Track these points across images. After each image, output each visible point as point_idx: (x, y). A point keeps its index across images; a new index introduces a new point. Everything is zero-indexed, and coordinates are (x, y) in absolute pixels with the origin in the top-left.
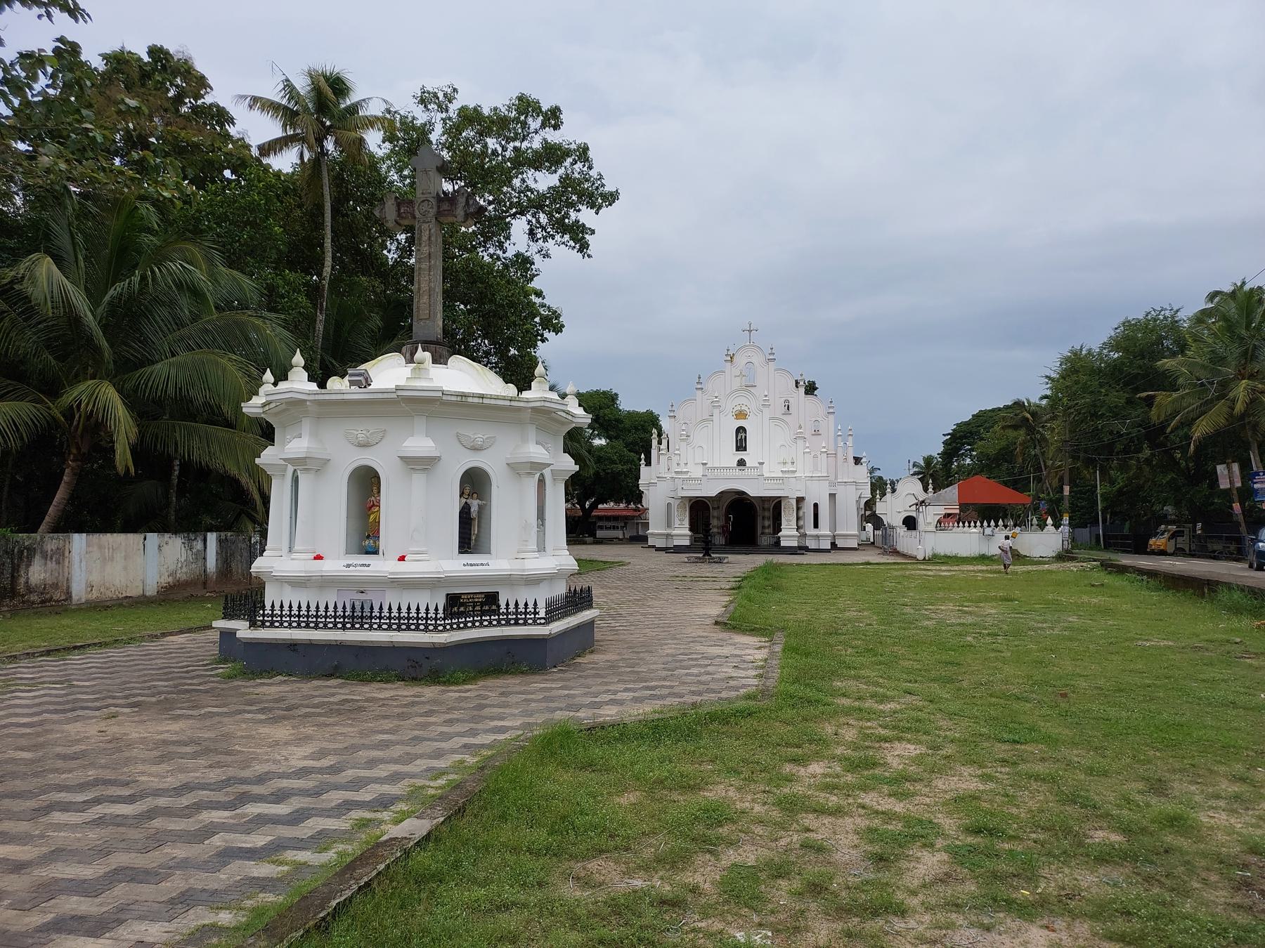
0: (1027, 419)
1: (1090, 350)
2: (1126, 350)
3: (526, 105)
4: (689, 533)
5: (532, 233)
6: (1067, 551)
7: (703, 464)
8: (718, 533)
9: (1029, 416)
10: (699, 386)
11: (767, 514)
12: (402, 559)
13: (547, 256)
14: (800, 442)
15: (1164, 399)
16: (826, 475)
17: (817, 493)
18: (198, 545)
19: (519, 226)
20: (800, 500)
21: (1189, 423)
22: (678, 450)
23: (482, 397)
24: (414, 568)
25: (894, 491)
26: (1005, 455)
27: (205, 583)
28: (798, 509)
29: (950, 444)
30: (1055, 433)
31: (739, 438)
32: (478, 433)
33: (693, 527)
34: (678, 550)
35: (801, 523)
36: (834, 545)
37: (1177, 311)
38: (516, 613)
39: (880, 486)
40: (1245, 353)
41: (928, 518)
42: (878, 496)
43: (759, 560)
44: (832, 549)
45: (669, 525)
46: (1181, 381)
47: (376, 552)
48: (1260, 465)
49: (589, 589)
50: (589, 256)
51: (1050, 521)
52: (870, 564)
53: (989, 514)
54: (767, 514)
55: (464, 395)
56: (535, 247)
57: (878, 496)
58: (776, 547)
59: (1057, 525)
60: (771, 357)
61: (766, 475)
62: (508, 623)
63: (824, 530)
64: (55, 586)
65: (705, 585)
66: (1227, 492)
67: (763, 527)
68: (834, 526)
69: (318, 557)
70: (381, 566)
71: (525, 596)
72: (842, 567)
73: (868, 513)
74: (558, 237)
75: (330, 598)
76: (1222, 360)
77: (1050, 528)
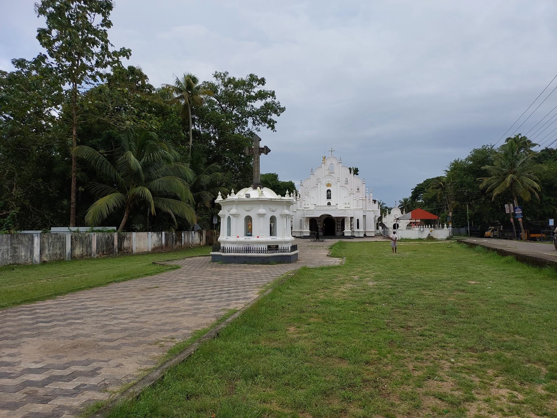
0: (441, 185)
1: (461, 160)
2: (474, 161)
3: (253, 78)
4: (309, 231)
5: (254, 123)
6: (451, 237)
7: (315, 205)
8: (320, 231)
9: (442, 184)
10: (312, 173)
11: (339, 223)
12: (258, 237)
13: (259, 131)
14: (352, 196)
15: (486, 180)
16: (362, 208)
17: (358, 215)
18: (160, 236)
19: (250, 120)
20: (352, 218)
21: (492, 190)
22: (304, 199)
23: (275, 199)
24: (260, 239)
25: (389, 213)
26: (434, 199)
27: (162, 248)
28: (351, 221)
29: (414, 193)
30: (450, 189)
31: (328, 194)
32: (273, 207)
33: (311, 229)
34: (305, 237)
35: (352, 227)
36: (365, 236)
37: (493, 146)
38: (284, 250)
39: (385, 211)
40: (511, 165)
41: (403, 224)
42: (383, 216)
43: (337, 241)
44: (364, 237)
45: (301, 228)
46: (492, 173)
47: (251, 235)
48: (517, 205)
49: (297, 245)
50: (276, 131)
51: (445, 225)
52: (377, 242)
53: (427, 222)
54: (339, 223)
55: (271, 199)
56: (254, 128)
57: (383, 216)
58: (343, 236)
59: (448, 227)
60: (340, 161)
61: (339, 208)
62: (282, 252)
63: (361, 229)
64: (129, 248)
65: (320, 248)
66: (509, 214)
67: (338, 228)
68: (365, 227)
69: (238, 237)
70: (253, 239)
71: (285, 246)
72: (366, 243)
73: (380, 222)
74: (263, 124)
75: (241, 246)
76: (504, 167)
77: (445, 228)
